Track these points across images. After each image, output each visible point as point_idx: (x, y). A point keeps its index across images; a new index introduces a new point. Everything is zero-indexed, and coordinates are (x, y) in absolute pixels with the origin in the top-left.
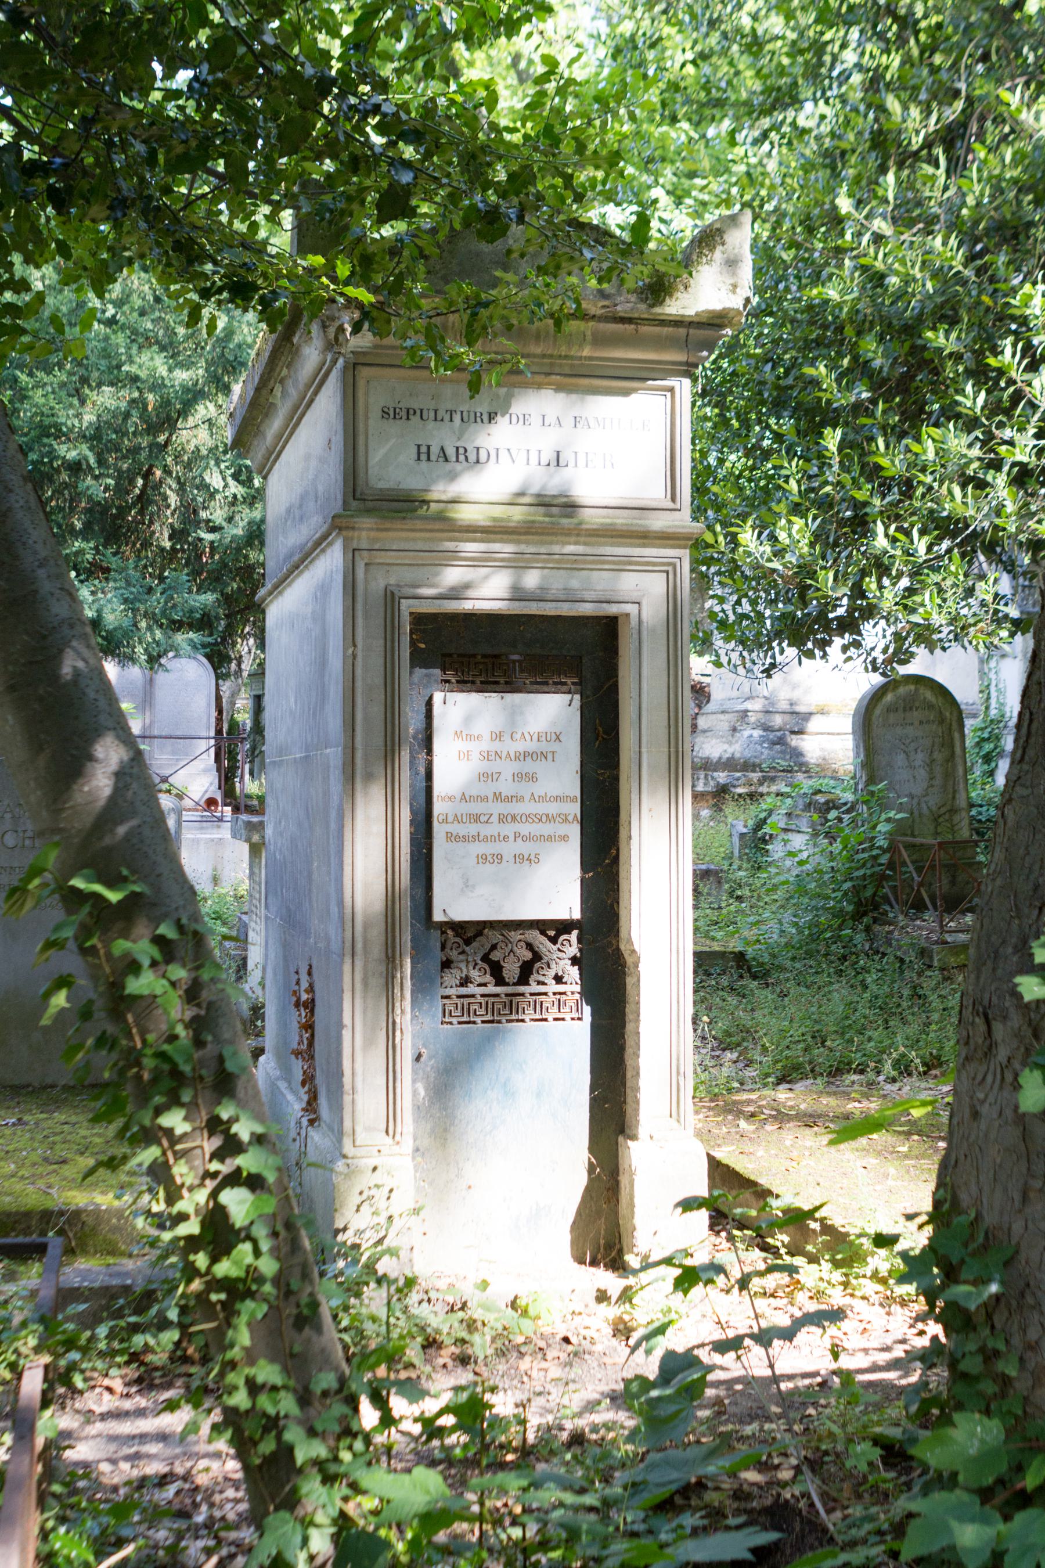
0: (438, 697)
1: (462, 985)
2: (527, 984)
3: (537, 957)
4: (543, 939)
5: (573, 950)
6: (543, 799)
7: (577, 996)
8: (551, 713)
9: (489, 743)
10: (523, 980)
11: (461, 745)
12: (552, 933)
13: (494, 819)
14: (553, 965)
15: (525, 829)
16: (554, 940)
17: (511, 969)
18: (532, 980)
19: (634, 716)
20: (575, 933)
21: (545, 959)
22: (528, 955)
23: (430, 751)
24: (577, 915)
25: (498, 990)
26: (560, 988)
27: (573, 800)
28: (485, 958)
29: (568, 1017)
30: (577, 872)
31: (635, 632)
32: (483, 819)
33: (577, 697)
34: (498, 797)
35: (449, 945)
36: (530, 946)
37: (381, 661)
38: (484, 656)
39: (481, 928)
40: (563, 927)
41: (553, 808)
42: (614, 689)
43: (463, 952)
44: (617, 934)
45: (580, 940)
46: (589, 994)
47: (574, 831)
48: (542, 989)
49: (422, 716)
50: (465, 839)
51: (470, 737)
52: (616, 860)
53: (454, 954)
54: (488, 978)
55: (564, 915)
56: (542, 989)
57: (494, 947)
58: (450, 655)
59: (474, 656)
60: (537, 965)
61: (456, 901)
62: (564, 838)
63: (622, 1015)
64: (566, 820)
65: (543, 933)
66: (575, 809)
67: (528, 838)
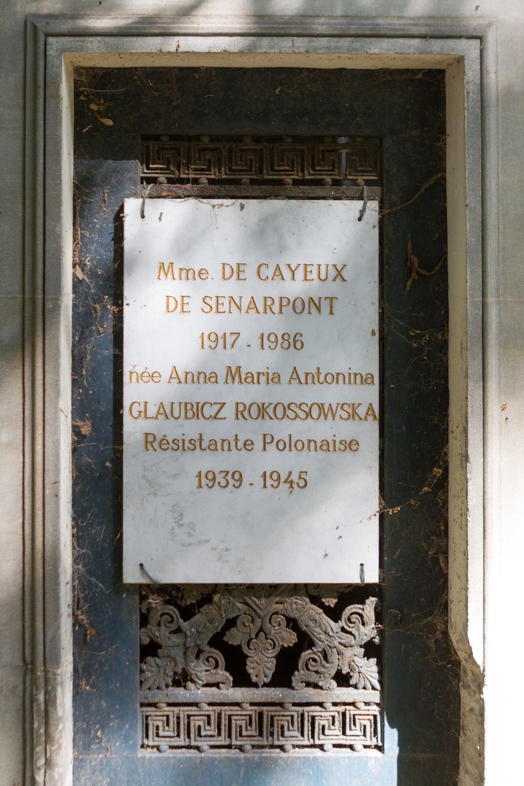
0: (132, 206)
1: (177, 683)
2: (288, 685)
3: (305, 641)
4: (316, 611)
5: (369, 631)
6: (314, 377)
7: (375, 710)
8: (336, 233)
9: (210, 286)
10: (282, 677)
11: (173, 287)
12: (331, 602)
13: (229, 411)
14: (334, 657)
15: (281, 429)
16: (335, 614)
17: (262, 663)
18: (297, 677)
19: (474, 240)
20: (372, 601)
21: (320, 646)
22: (290, 638)
23: (118, 299)
24: (373, 577)
25: (239, 694)
26: (345, 694)
27: (366, 380)
28: (217, 642)
29: (358, 745)
30: (372, 503)
31: (474, 96)
32: (209, 411)
33: (373, 205)
34: (234, 374)
35: (154, 618)
36: (292, 623)
37: (17, 145)
38: (214, 139)
39: (207, 593)
40: (355, 593)
41: (332, 394)
42: (439, 191)
43: (178, 631)
44: (445, 608)
45: (379, 618)
46: (396, 707)
47: (369, 435)
48: (312, 694)
49: (108, 239)
50: (179, 445)
51: (187, 273)
52: (442, 484)
53: (162, 634)
54: (223, 674)
55: (352, 578)
56: (312, 694)
57: (231, 623)
58: (157, 138)
59: (197, 138)
60: (306, 655)
61: (162, 548)
62: (351, 445)
63: (454, 747)
64: (353, 415)
65: (316, 600)
66: (370, 395)
67: (289, 445)
